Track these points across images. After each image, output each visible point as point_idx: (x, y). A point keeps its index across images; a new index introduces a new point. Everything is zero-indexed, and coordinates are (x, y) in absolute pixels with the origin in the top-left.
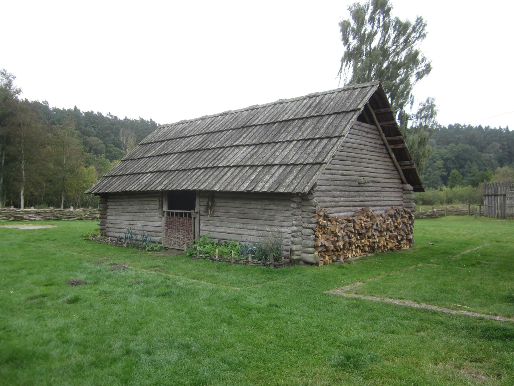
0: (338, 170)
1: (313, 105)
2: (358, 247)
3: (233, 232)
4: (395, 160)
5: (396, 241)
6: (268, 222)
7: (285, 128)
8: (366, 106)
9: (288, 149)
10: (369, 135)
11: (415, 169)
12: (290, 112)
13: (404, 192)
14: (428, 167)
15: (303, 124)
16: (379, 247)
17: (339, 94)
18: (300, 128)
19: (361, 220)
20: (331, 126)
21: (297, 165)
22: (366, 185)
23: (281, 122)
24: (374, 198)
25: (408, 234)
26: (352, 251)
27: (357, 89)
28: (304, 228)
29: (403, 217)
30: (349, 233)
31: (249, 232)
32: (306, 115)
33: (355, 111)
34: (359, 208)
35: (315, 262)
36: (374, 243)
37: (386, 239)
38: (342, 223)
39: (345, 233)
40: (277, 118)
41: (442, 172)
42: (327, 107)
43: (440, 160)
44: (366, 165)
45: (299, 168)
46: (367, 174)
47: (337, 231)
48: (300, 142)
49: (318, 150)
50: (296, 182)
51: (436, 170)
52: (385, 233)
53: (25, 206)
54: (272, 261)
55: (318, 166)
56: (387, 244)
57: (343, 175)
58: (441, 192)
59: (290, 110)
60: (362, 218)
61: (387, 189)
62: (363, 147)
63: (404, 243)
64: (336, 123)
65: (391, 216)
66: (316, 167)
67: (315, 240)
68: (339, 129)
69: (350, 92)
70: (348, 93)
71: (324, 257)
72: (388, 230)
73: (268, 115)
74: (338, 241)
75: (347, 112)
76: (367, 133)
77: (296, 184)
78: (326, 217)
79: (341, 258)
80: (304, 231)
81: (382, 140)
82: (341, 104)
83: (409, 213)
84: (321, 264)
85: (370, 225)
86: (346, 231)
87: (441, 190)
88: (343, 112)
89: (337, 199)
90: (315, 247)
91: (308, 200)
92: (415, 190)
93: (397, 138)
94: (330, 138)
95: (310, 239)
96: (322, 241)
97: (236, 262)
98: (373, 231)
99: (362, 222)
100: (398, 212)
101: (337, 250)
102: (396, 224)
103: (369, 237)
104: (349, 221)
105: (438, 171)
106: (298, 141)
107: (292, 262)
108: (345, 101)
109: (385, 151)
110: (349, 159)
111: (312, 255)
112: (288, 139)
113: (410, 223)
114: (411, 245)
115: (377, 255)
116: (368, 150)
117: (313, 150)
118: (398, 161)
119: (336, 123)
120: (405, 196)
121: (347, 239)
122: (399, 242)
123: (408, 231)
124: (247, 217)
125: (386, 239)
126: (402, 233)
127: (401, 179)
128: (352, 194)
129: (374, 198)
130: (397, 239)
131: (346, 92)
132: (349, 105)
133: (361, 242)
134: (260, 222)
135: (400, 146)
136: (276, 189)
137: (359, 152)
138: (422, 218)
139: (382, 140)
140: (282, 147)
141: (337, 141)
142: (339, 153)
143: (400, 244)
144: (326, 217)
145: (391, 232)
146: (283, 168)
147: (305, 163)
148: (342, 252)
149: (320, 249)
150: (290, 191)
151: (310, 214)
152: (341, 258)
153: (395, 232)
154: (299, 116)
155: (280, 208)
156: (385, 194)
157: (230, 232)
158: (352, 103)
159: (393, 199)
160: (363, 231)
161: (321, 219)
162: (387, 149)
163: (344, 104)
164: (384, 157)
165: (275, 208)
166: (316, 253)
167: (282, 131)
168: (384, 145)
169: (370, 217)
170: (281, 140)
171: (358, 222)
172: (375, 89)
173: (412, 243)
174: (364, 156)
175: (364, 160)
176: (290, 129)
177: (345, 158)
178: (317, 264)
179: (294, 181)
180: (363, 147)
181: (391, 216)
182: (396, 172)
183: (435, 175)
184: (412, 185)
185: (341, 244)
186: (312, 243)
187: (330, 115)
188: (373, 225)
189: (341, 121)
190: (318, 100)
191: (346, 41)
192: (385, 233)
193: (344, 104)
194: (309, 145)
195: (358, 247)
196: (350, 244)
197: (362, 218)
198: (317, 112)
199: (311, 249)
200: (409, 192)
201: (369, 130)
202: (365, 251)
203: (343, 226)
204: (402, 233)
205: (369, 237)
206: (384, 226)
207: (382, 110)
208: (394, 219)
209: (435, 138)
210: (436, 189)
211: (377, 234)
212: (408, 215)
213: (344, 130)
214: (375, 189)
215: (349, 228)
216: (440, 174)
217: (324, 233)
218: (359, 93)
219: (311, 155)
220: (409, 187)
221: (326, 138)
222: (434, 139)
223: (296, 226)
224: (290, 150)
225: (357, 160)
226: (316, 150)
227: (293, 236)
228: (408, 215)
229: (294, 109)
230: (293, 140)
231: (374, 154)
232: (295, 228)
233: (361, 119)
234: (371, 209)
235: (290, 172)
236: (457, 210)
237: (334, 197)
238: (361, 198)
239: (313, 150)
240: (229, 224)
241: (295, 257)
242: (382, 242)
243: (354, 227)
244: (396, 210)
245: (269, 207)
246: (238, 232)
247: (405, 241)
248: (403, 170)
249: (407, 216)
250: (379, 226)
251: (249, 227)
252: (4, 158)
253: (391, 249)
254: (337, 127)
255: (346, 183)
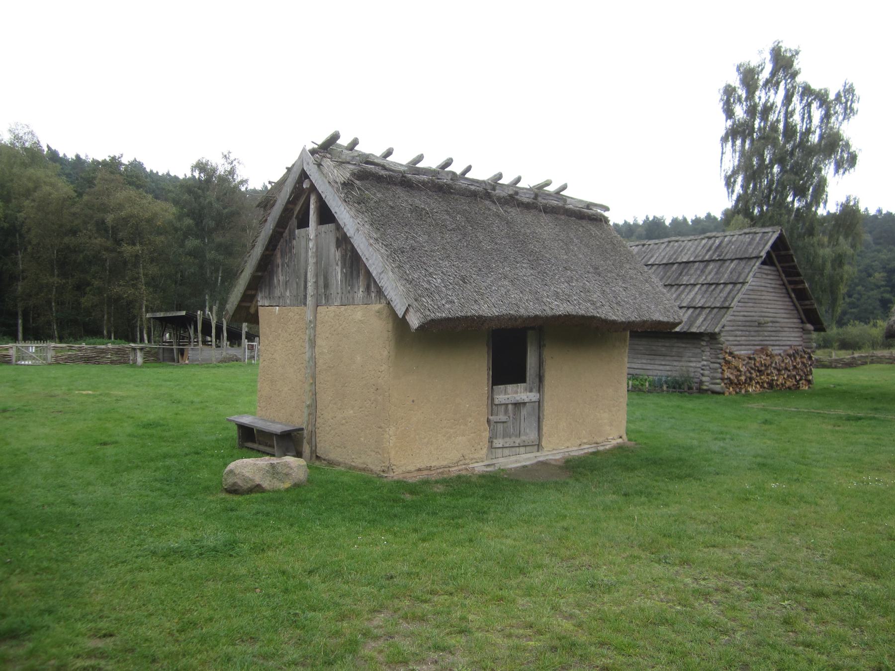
0: (740, 312)
1: (713, 248)
2: (758, 383)
3: (639, 367)
4: (795, 300)
5: (794, 380)
6: (675, 358)
7: (686, 270)
8: (768, 253)
9: (693, 293)
10: (769, 277)
11: (816, 309)
12: (689, 253)
13: (804, 332)
14: (857, 285)
15: (706, 267)
16: (777, 385)
17: (740, 237)
18: (703, 271)
19: (760, 358)
20: (734, 272)
21: (705, 308)
22: (765, 325)
23: (680, 263)
24: (772, 338)
25: (808, 375)
26: (752, 386)
27: (758, 233)
28: (712, 363)
29: (802, 357)
30: (750, 369)
31: (657, 367)
32: (707, 258)
33: (757, 257)
34: (758, 348)
35: (722, 391)
36: (773, 380)
37: (784, 378)
38: (744, 360)
39: (746, 369)
40: (676, 259)
41: (882, 293)
42: (728, 251)
43: (880, 273)
44: (766, 306)
45: (707, 311)
46: (767, 314)
47: (740, 366)
48: (705, 286)
49: (724, 294)
50: (706, 324)
51: (872, 290)
52: (783, 372)
53: (248, 345)
54: (686, 389)
55: (725, 310)
56: (785, 382)
57: (744, 316)
58: (874, 329)
59: (688, 250)
60: (762, 356)
61: (786, 329)
62: (763, 288)
63: (803, 384)
64: (739, 269)
65: (790, 356)
66: (724, 311)
67: (722, 373)
68: (743, 276)
69: (751, 237)
70: (749, 237)
71: (729, 389)
72: (786, 369)
73: (663, 254)
74: (740, 375)
75: (750, 259)
76: (767, 274)
77: (707, 325)
78: (731, 354)
79: (743, 391)
80: (712, 366)
81: (782, 280)
82: (743, 250)
83: (809, 354)
84: (727, 394)
85: (769, 363)
86: (748, 367)
87: (875, 325)
88: (746, 258)
89: (738, 339)
90: (722, 379)
91: (716, 339)
92: (815, 330)
93: (797, 279)
94: (735, 284)
95: (718, 372)
96: (728, 374)
97: (649, 392)
98: (772, 369)
99: (762, 360)
100: (797, 352)
101: (740, 384)
102: (795, 364)
103: (768, 375)
104: (750, 358)
105: (875, 292)
106: (703, 285)
107: (701, 391)
108: (747, 246)
109: (784, 291)
110: (750, 301)
111: (719, 386)
112: (692, 282)
113: (810, 363)
114: (810, 386)
115: (775, 391)
116: (768, 292)
117: (719, 295)
118: (798, 300)
119: (739, 269)
120: (805, 336)
121: (748, 375)
122: (798, 382)
123: (807, 371)
124: (654, 354)
125: (784, 378)
126: (801, 373)
127: (801, 319)
128: (753, 333)
129: (772, 338)
130: (796, 378)
131: (747, 236)
132: (751, 251)
133: (761, 379)
134: (668, 358)
135: (800, 286)
136: (688, 329)
137: (759, 294)
138: (836, 367)
139: (782, 280)
140: (687, 290)
141: (741, 287)
142: (744, 296)
143: (798, 384)
144: (731, 354)
145: (789, 371)
146: (691, 311)
147: (713, 306)
148: (743, 386)
149: (726, 381)
150: (702, 331)
151: (718, 351)
152: (743, 391)
153: (793, 371)
154: (700, 258)
155: (688, 345)
156: (784, 334)
157: (636, 367)
158: (754, 249)
159: (792, 339)
160: (763, 368)
161: (727, 356)
162: (787, 289)
163: (746, 250)
164: (784, 297)
165: (683, 345)
166: (723, 384)
167: (684, 273)
168: (784, 284)
169: (769, 356)
170: (684, 283)
171: (758, 360)
172: (776, 236)
173: (811, 384)
174: (763, 297)
175: (764, 302)
176: (692, 271)
177: (746, 300)
178: (723, 393)
179: (704, 323)
180: (763, 288)
181: (790, 356)
182: (795, 312)
183: (869, 297)
184: (812, 324)
185: (743, 378)
186: (719, 375)
187: (732, 260)
188: (772, 363)
189: (744, 268)
190: (717, 242)
191: (729, 113)
192: (783, 372)
193: (746, 250)
194: (714, 289)
195: (758, 383)
196: (751, 379)
197: (762, 356)
198: (719, 256)
199: (718, 381)
200: (808, 332)
201: (769, 272)
202: (764, 388)
203: (745, 363)
204: (801, 373)
205: (768, 375)
206: (783, 365)
207: (783, 253)
208: (793, 358)
209: (870, 232)
210: (866, 323)
211: (775, 372)
212: (808, 355)
213: (747, 276)
214: (774, 329)
215: (750, 365)
216: (879, 297)
217: (729, 368)
218: (761, 239)
219: (717, 299)
220: (809, 327)
221: (731, 283)
222: (869, 235)
223: (706, 361)
224: (696, 294)
225: (757, 301)
226: (721, 295)
227: (703, 369)
228: (808, 355)
229: (692, 249)
230: (697, 284)
231: (773, 294)
232: (705, 363)
233: (764, 263)
234: (770, 348)
235: (699, 315)
236: (890, 356)
237: (736, 336)
238: (760, 338)
239: (719, 295)
240: (635, 360)
241: (705, 387)
242: (780, 380)
243: (754, 364)
244: (795, 350)
245: (677, 345)
246: (645, 367)
247: (803, 381)
248: (803, 310)
249: (806, 356)
250: (778, 364)
251: (657, 362)
252: (220, 275)
253: (789, 388)
254: (740, 274)
255: (748, 324)
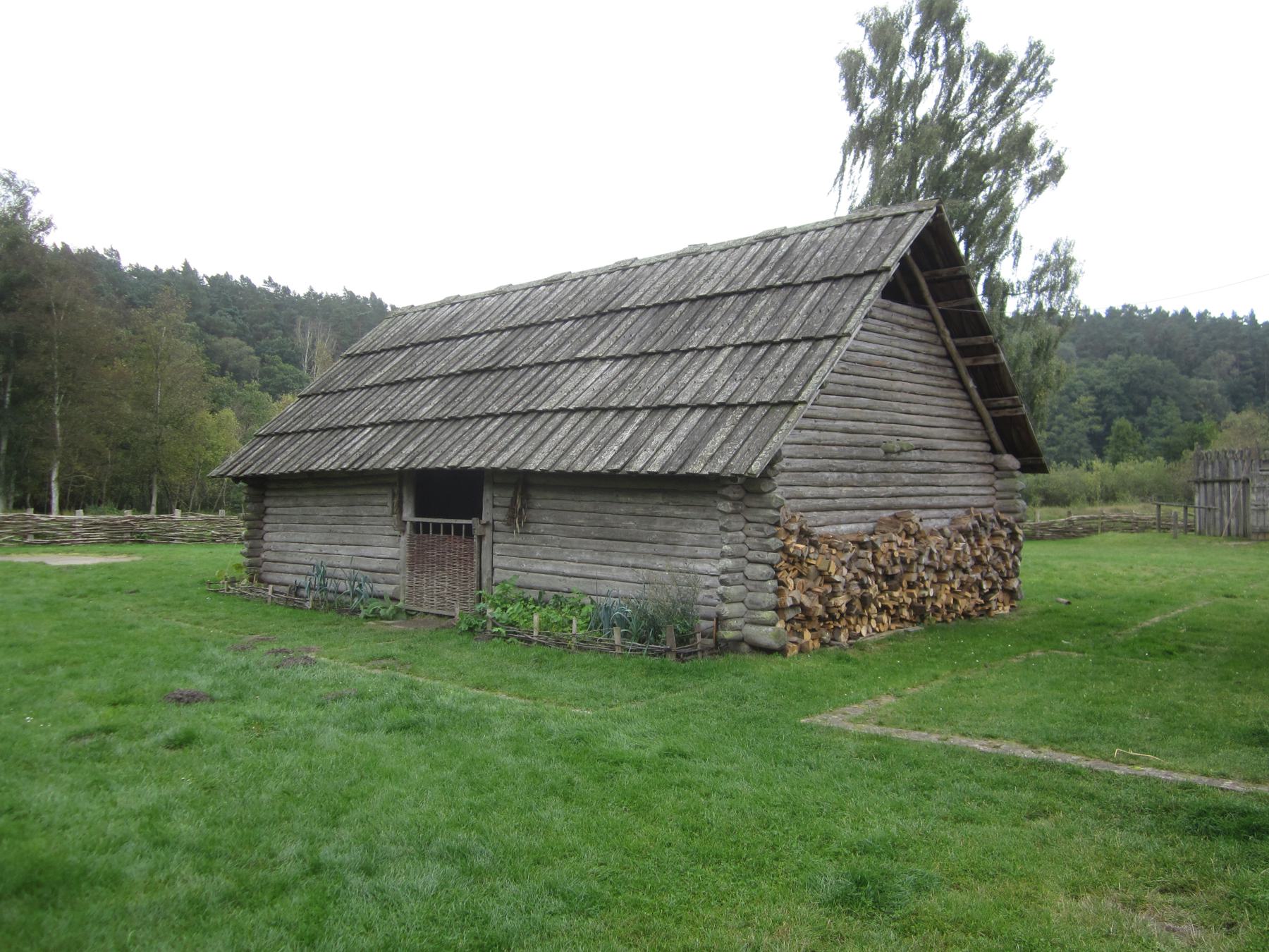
0: (834, 420)
1: (773, 260)
2: (884, 609)
3: (576, 571)
4: (976, 395)
5: (976, 594)
6: (661, 548)
7: (703, 316)
8: (903, 261)
9: (711, 368)
10: (911, 334)
11: (1024, 416)
12: (716, 276)
13: (997, 473)
14: (1056, 413)
15: (749, 305)
16: (936, 610)
17: (838, 231)
18: (740, 315)
19: (890, 541)
20: (816, 312)
21: (734, 406)
22: (903, 455)
23: (693, 301)
24: (923, 489)
25: (1008, 578)
26: (870, 618)
27: (881, 218)
28: (750, 562)
29: (994, 535)
30: (861, 575)
31: (615, 572)
32: (755, 283)
33: (876, 273)
34: (886, 514)
35: (777, 646)
36: (923, 599)
37: (952, 590)
38: (846, 551)
39: (851, 576)
40: (684, 291)
41: (1090, 424)
42: (808, 263)
43: (1086, 396)
44: (904, 407)
45: (738, 413)
46: (906, 429)
47: (833, 569)
48: (742, 350)
49: (785, 369)
50: (730, 449)
51: (1077, 419)
52: (951, 575)
53: (62, 508)
54: (671, 643)
55: (785, 409)
56: (956, 601)
57: (846, 431)
58: (1089, 473)
59: (715, 272)
60: (895, 537)
61: (955, 467)
62: (896, 362)
63: (997, 600)
64: (830, 302)
65: (966, 533)
66: (780, 412)
67: (778, 593)
68: (838, 319)
69: (863, 228)
70: (859, 229)
71: (801, 635)
72: (957, 566)
73: (660, 283)
74: (834, 594)
75: (857, 277)
76: (907, 327)
77: (731, 454)
78: (804, 535)
79: (843, 637)
80: (751, 570)
81: (944, 345)
82: (843, 257)
83: (1009, 525)
84: (793, 651)
85: (914, 555)
86: (855, 570)
87: (1089, 469)
88: (847, 276)
89: (831, 491)
90: (778, 609)
91: (760, 493)
92: (1025, 469)
93: (980, 340)
94: (815, 340)
95: (765, 590)
96: (796, 594)
97: (583, 646)
98: (921, 569)
99: (895, 548)
100: (982, 522)
101: (832, 617)
102: (978, 553)
103: (911, 585)
104: (862, 545)
105: (1081, 423)
106: (737, 347)
107: (722, 647)
108: (852, 250)
109: (950, 372)
110: (861, 391)
111: (770, 629)
112: (712, 342)
113: (1012, 549)
114: (1015, 603)
115: (931, 629)
116: (908, 371)
117: (772, 371)
118: (983, 396)
119: (830, 302)
120: (999, 484)
121: (856, 590)
122: (985, 596)
123: (1008, 569)
124: (610, 536)
125: (952, 590)
126: (993, 574)
127: (990, 442)
128: (870, 477)
129: (923, 489)
130: (981, 589)
131: (855, 227)
132: (862, 260)
133: (892, 598)
134: (641, 547)
135: (988, 361)
136: (681, 467)
137: (887, 375)
138: (1042, 538)
139: (944, 345)
140: (697, 364)
141: (833, 348)
142: (837, 377)
143: (987, 602)
144: (804, 535)
145: (965, 571)
146: (698, 414)
147: (753, 401)
148: (844, 622)
149: (790, 615)
150: (716, 471)
151: (766, 527)
152: (843, 637)
153: (975, 571)
154: (738, 286)
155: (690, 512)
156: (951, 478)
157: (568, 571)
158: (868, 255)
159: (970, 490)
160: (897, 570)
161: (793, 540)
162: (955, 368)
163: (850, 257)
164: (949, 387)
165: (678, 512)
166: (781, 625)
167: (696, 324)
168: (949, 357)
169: (914, 535)
170: (694, 345)
171: (883, 547)
172: (925, 219)
173: (1017, 599)
174: (898, 385)
175: (899, 395)
176: (715, 318)
177: (852, 390)
178: (783, 651)
179: (727, 446)
180: (896, 362)
181: (966, 533)
182: (977, 425)
183: (1073, 431)
184: (1017, 456)
185: (841, 601)
186: (771, 599)
187: (814, 284)
188: (920, 554)
189: (841, 300)
190: (784, 247)
191: (854, 101)
192: (951, 575)
193: (850, 257)
194: (763, 357)
195: (884, 609)
196: (865, 601)
197: (895, 537)
198: (782, 276)
199: (768, 615)
200: (1009, 473)
201: (911, 322)
202: (902, 620)
203: (846, 558)
204: (993, 574)
205: (911, 585)
206: (949, 558)
207: (944, 272)
208: (972, 539)
209: (1073, 341)
210: (1076, 465)
211: (930, 576)
212: (1008, 530)
213: (848, 319)
214: (925, 466)
215: (862, 563)
216: (1087, 429)
217: (800, 575)
218: (887, 230)
219: (768, 381)
220: (1010, 461)
221: (806, 339)
222: (1071, 344)
223: (732, 557)
224: (717, 371)
225: (882, 394)
226: (780, 370)
227: (723, 582)
228: (1008, 530)
229: (725, 268)
230: (724, 346)
231: (923, 379)
232: (729, 563)
233: (890, 293)
234: (916, 515)
235: (716, 424)
236: (1129, 518)
237: (825, 486)
238: (891, 490)
239: (772, 371)
240: (566, 552)
241: (729, 635)
242: (944, 597)
243: (874, 560)
244: (977, 518)
245: (663, 511)
246: (588, 573)
247: (999, 595)
248: (994, 419)
249: (1004, 533)
250: (936, 558)
251: (615, 560)
252: (9, 390)
253: (966, 615)
254: (831, 314)
255: (855, 452)
